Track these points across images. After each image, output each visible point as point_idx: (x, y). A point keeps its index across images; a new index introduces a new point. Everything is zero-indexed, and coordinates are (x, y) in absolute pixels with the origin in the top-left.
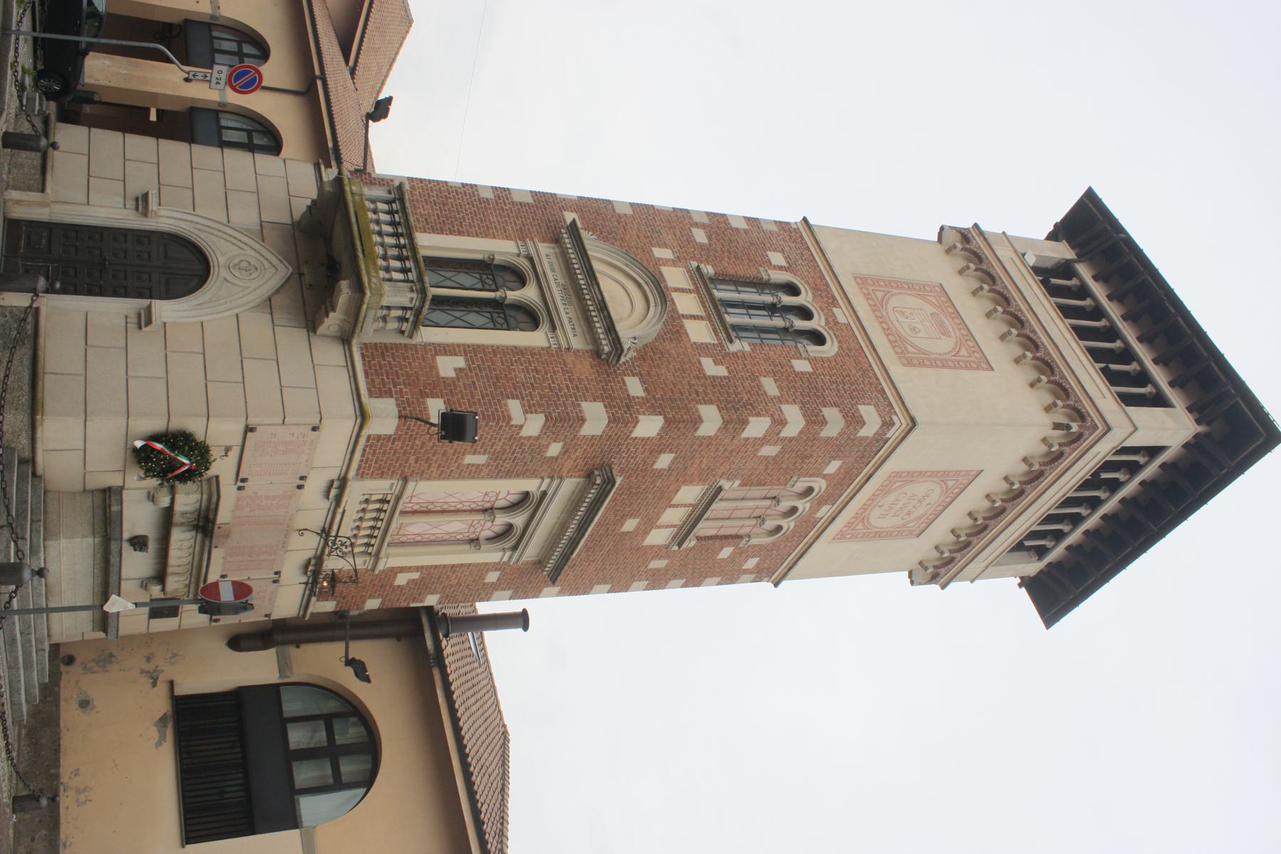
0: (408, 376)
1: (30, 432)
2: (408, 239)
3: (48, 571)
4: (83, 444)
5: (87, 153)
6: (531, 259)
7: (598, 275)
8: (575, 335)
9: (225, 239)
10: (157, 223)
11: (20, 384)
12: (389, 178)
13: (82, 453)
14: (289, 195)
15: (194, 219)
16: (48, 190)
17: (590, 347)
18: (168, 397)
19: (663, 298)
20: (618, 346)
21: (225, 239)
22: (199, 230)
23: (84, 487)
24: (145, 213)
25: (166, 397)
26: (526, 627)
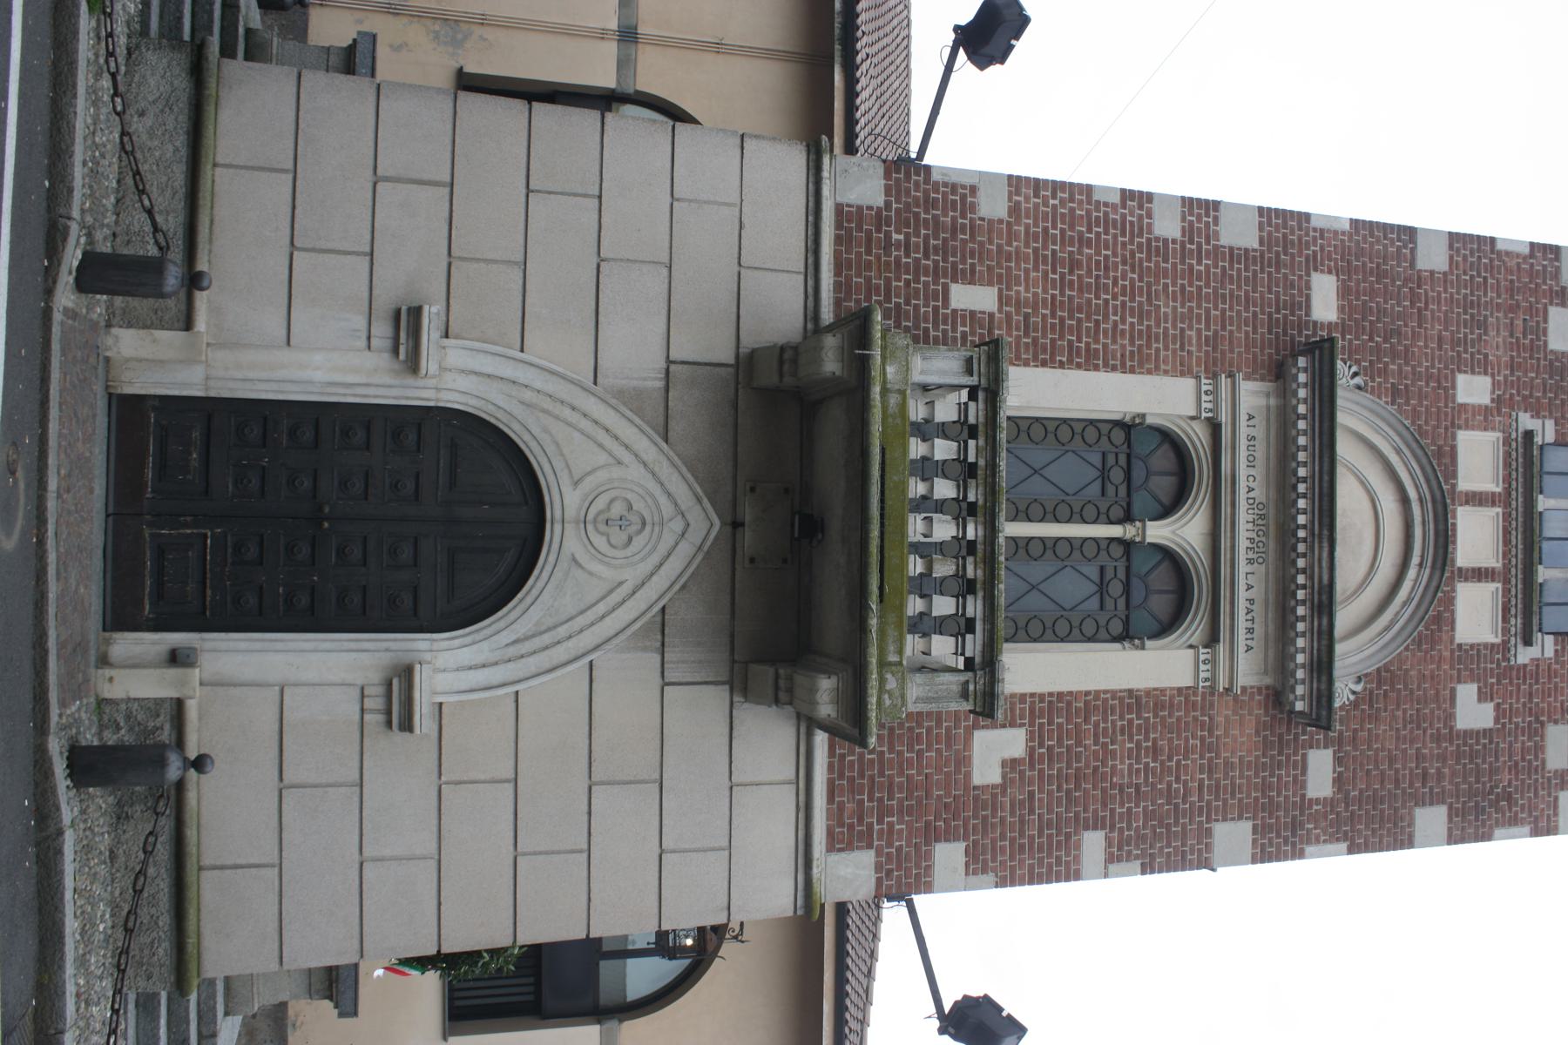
0: (911, 786)
2: (985, 524)
3: (213, 762)
5: (290, 166)
6: (1215, 428)
7: (1340, 471)
8: (1249, 649)
9: (582, 432)
10: (438, 389)
11: (153, 911)
12: (967, 181)
14: (740, 265)
15: (522, 374)
16: (201, 324)
17: (1268, 681)
18: (439, 904)
19: (1441, 551)
20: (1324, 713)
21: (582, 432)
22: (529, 405)
24: (413, 365)
25: (435, 902)
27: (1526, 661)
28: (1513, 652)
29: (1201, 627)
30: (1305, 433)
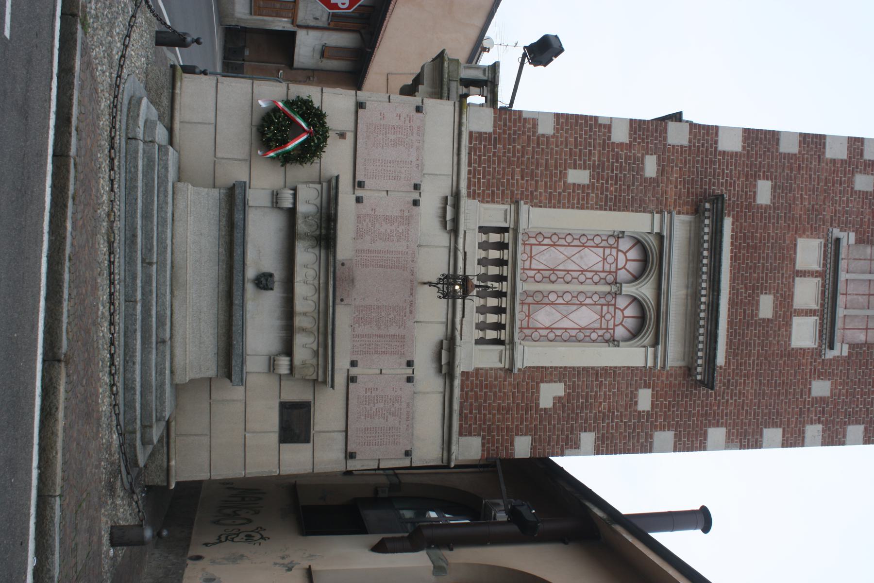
1: (170, 91)
4: (214, 118)
13: (213, 127)
23: (181, 435)
26: (706, 528)
27: (831, 357)
28: (823, 352)
29: (650, 336)
30: (706, 273)
